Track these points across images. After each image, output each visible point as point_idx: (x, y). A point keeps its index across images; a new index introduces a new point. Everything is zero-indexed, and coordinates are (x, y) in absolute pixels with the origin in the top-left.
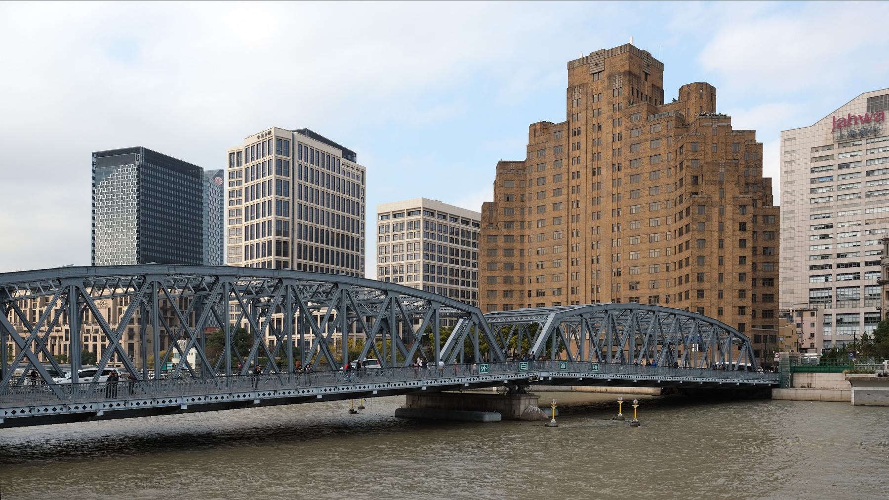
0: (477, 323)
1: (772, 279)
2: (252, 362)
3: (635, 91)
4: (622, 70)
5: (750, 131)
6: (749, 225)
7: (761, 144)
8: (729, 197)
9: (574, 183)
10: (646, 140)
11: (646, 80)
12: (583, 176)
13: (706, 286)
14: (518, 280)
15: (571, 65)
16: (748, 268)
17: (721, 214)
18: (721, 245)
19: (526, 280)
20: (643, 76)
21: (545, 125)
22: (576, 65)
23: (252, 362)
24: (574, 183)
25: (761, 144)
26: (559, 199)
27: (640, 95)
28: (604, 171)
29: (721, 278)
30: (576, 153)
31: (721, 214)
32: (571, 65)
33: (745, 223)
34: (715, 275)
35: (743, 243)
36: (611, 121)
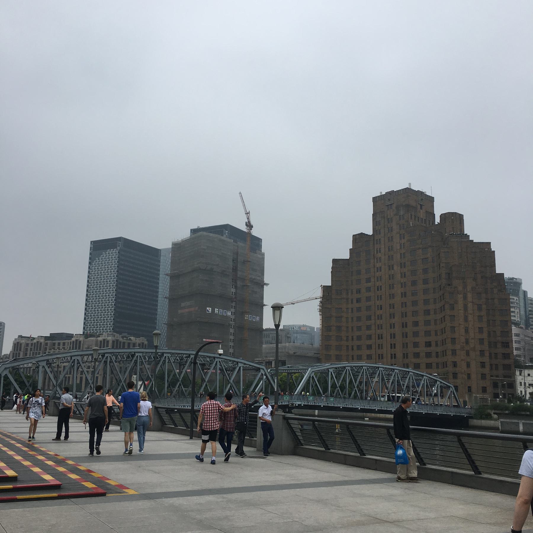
0: (264, 374)
1: (508, 343)
2: (178, 371)
3: (413, 217)
4: (404, 204)
5: (487, 243)
6: (484, 306)
7: (494, 252)
8: (469, 288)
9: (378, 274)
10: (419, 248)
11: (421, 208)
12: (383, 270)
13: (458, 347)
14: (345, 339)
15: (375, 199)
16: (485, 336)
17: (465, 298)
18: (466, 319)
19: (350, 338)
20: (419, 207)
21: (362, 235)
22: (377, 199)
23: (178, 371)
24: (378, 274)
25: (494, 252)
26: (369, 284)
27: (417, 219)
28: (395, 267)
29: (467, 342)
30: (379, 255)
31: (465, 298)
32: (375, 199)
33: (481, 305)
34: (463, 339)
35: (480, 317)
36: (398, 235)
